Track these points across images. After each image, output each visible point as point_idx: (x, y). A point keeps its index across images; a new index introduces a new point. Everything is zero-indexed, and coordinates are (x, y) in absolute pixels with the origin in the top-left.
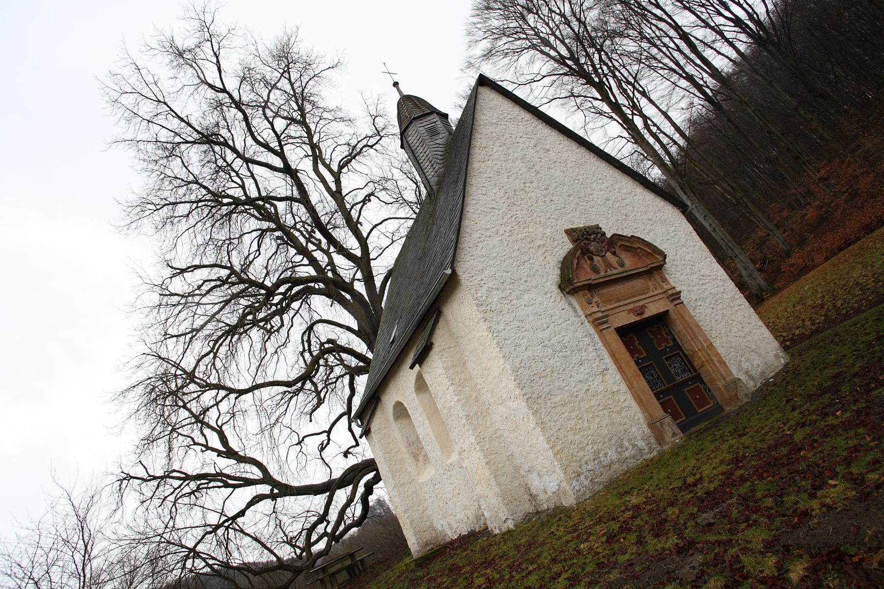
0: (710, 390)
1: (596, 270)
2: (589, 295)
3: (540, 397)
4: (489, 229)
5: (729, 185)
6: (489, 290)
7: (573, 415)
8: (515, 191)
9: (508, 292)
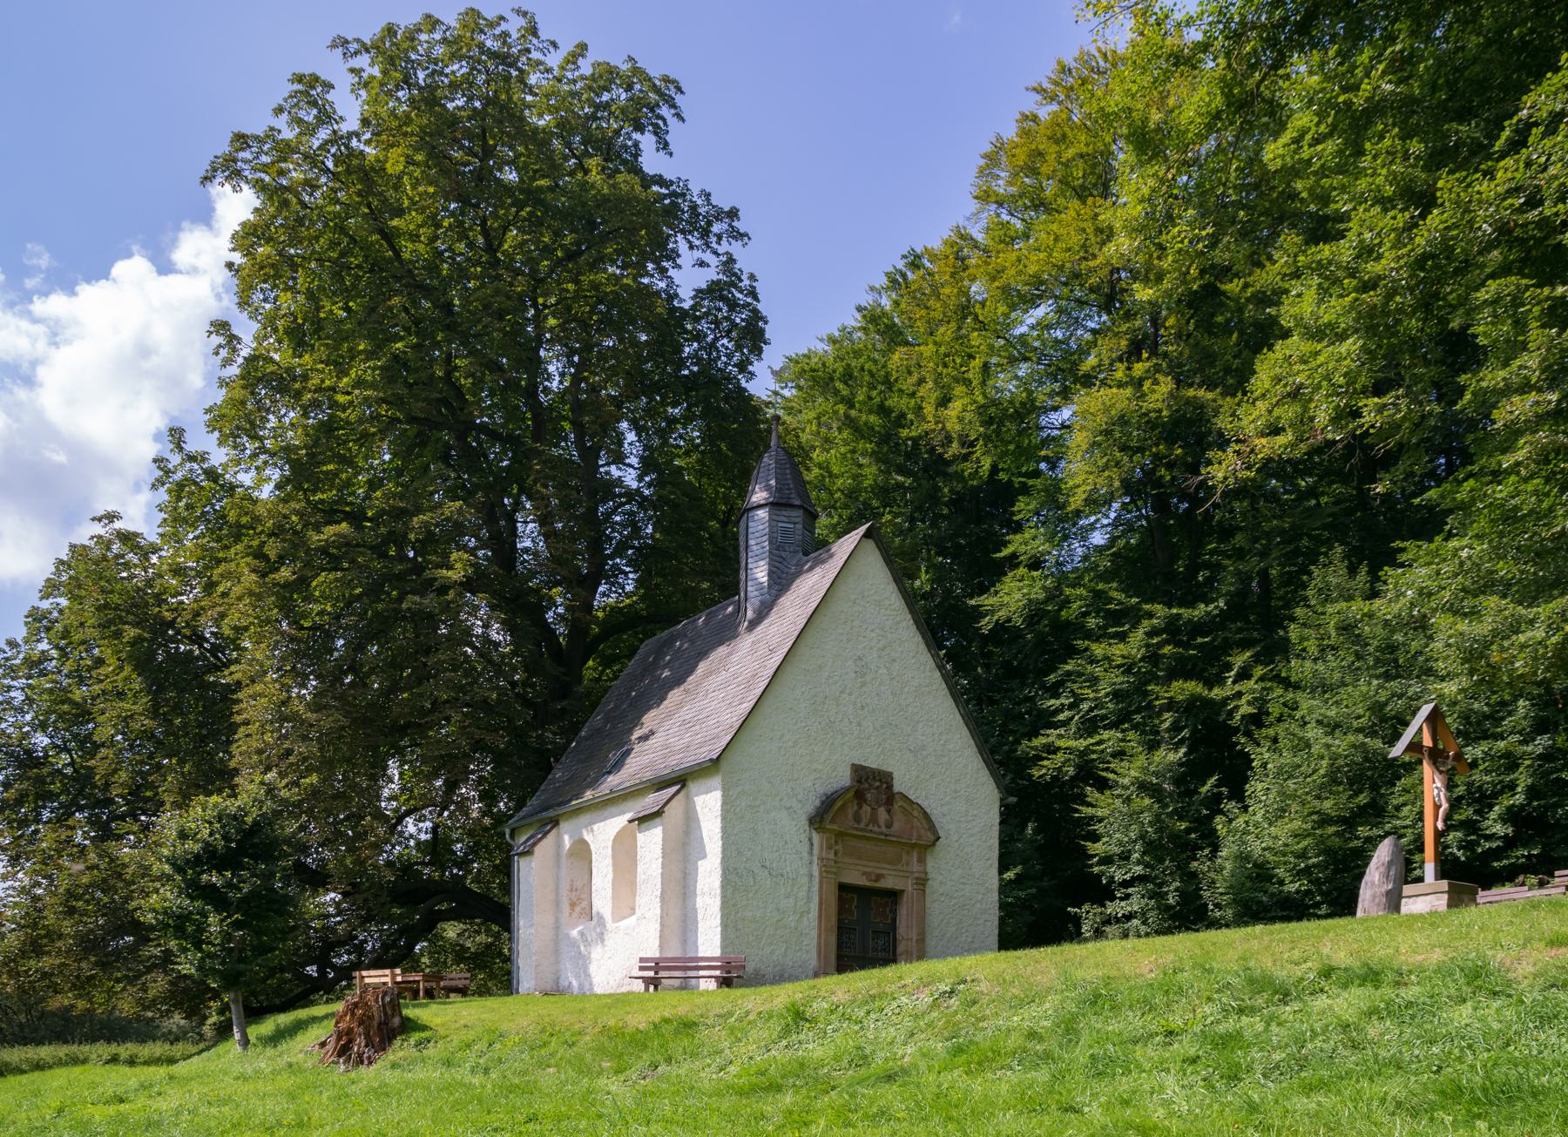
1: (857, 819)
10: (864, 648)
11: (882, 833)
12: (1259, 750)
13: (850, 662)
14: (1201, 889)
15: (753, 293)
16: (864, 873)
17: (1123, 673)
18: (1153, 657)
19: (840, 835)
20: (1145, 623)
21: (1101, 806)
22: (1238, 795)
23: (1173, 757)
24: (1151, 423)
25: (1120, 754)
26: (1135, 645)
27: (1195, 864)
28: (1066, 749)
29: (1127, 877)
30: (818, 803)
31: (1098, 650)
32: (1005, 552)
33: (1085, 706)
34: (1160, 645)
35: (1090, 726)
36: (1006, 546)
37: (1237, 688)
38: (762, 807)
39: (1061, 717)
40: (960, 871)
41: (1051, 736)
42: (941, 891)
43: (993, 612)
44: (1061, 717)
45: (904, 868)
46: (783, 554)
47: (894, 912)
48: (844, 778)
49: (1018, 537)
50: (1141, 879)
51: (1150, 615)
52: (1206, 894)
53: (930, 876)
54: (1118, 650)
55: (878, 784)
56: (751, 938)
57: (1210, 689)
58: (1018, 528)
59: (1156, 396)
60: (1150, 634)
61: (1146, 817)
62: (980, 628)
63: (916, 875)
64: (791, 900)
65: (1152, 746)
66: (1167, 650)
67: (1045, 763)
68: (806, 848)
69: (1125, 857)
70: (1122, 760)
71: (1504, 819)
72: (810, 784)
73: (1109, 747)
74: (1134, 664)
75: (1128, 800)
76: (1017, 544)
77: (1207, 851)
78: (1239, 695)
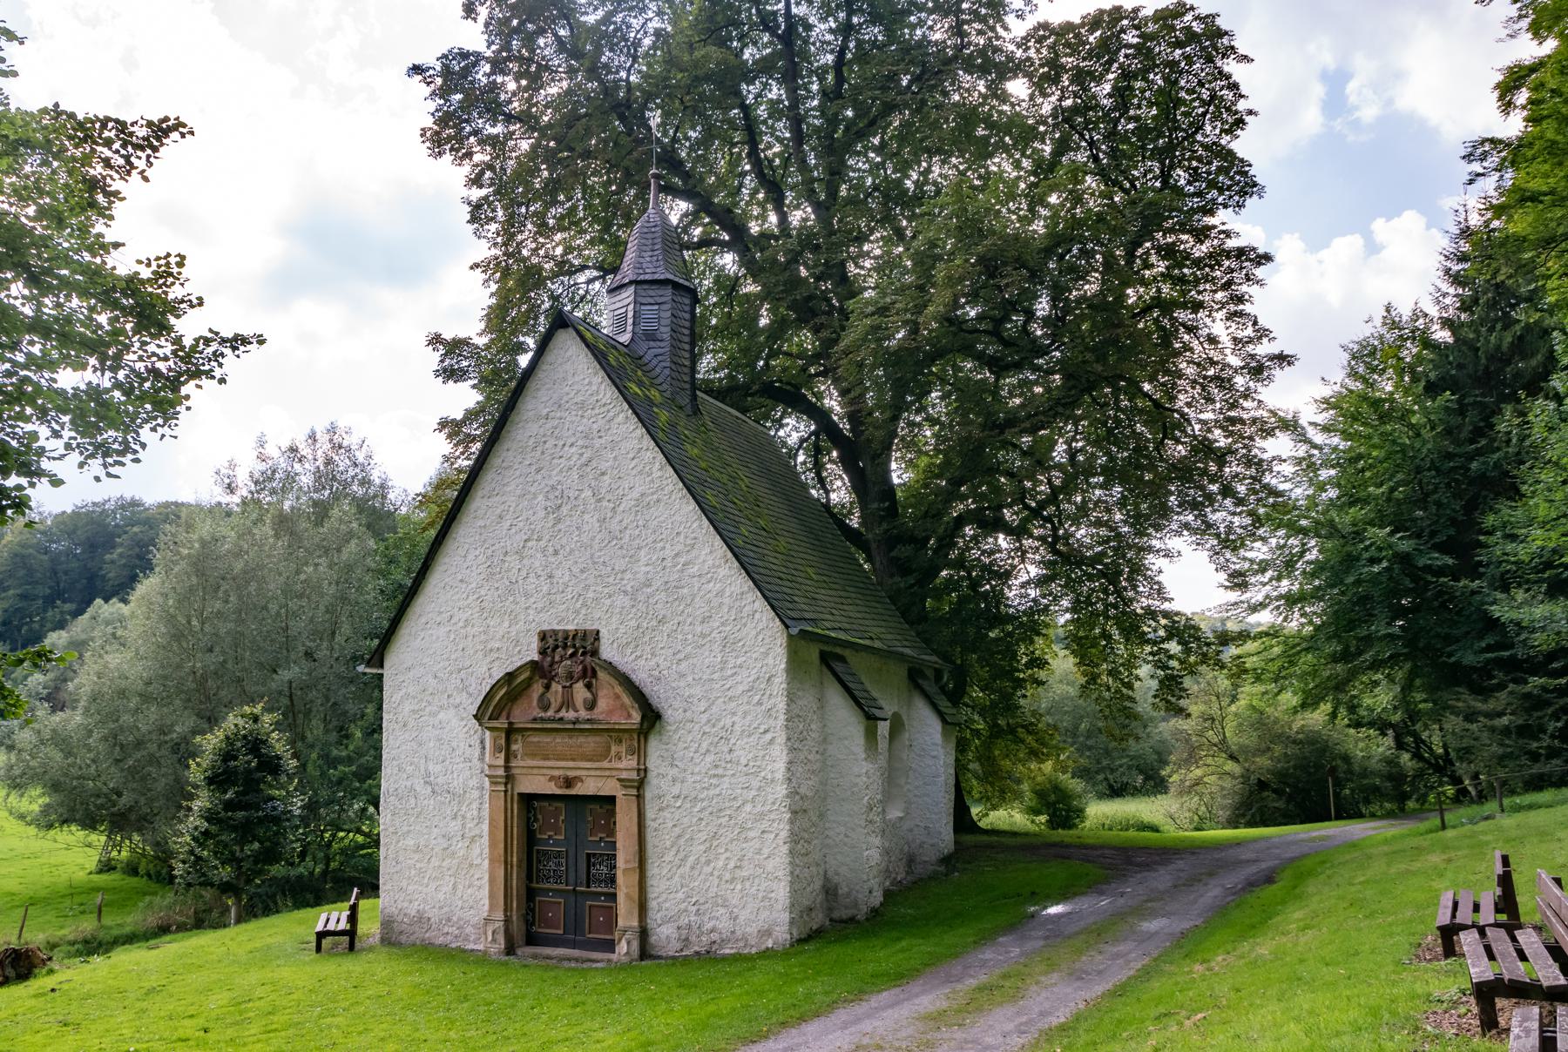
16: (552, 778)
42: (675, 791)
48: (530, 652)
56: (413, 872)
68: (477, 753)
72: (485, 668)
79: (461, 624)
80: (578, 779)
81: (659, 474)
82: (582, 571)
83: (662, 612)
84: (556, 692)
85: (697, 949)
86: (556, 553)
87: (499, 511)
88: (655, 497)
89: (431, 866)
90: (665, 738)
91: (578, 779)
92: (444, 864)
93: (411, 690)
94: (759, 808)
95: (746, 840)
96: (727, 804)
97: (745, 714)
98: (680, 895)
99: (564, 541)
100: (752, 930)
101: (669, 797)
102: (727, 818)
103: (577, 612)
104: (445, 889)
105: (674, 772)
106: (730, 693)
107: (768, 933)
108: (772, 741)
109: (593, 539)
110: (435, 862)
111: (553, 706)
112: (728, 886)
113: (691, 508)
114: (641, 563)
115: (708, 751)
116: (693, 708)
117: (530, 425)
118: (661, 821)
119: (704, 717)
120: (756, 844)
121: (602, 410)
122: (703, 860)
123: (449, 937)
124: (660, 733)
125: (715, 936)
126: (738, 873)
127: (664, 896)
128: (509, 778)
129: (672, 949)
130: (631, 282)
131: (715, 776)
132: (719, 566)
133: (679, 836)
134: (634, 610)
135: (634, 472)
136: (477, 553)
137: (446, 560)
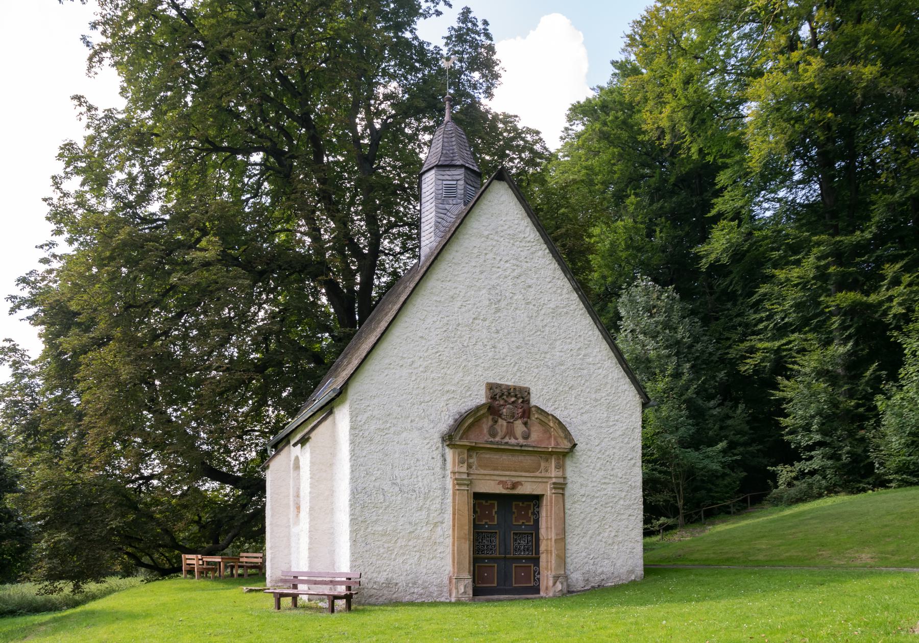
0: (539, 573)
1: (493, 434)
2: (466, 456)
3: (366, 521)
4: (405, 358)
5: (246, 557)
6: (372, 417)
7: (386, 545)
8: (459, 325)
9: (388, 425)
10: (499, 277)
11: (518, 445)
12: (909, 340)
13: (484, 291)
14: (869, 451)
15: (488, 36)
16: (501, 482)
17: (801, 289)
18: (822, 275)
19: (471, 449)
20: (815, 250)
21: (788, 389)
22: (893, 377)
23: (842, 350)
24: (807, 94)
25: (802, 351)
26: (809, 266)
27: (862, 432)
28: (764, 349)
29: (810, 443)
30: (451, 421)
31: (781, 274)
32: (713, 212)
33: (778, 317)
34: (827, 266)
35: (782, 330)
36: (713, 208)
37: (890, 293)
38: (392, 430)
39: (761, 326)
40: (601, 473)
41: (754, 341)
42: (582, 492)
43: (707, 256)
44: (761, 326)
45: (543, 474)
46: (447, 207)
47: (537, 514)
48: (480, 398)
49: (720, 199)
50: (820, 444)
51: (818, 244)
52: (873, 455)
53: (569, 481)
54: (795, 273)
55: (513, 399)
56: (382, 550)
57: (868, 296)
58: (719, 193)
59: (809, 74)
60: (819, 259)
61: (823, 397)
62: (700, 268)
63: (554, 480)
64: (424, 512)
65: (827, 343)
66: (832, 269)
67: (748, 361)
68: (439, 463)
69: (807, 428)
70: (804, 355)
71: (721, 162)
72: (443, 404)
73: (795, 346)
74: (808, 282)
75: (809, 385)
76: (720, 205)
77: (872, 422)
78: (890, 299)
79: (421, 369)
80: (519, 483)
81: (567, 296)
82: (518, 348)
83: (572, 383)
84: (502, 425)
85: (593, 584)
86: (498, 332)
87: (451, 293)
88: (565, 310)
89: (398, 545)
90: (575, 460)
91: (519, 483)
92: (410, 543)
93: (376, 413)
94: (627, 502)
95: (621, 520)
96: (611, 500)
97: (621, 448)
98: (584, 554)
99: (503, 325)
100: (624, 570)
101: (578, 495)
102: (610, 508)
103: (515, 375)
104: (410, 562)
105: (581, 480)
106: (611, 436)
107: (631, 572)
108: (634, 465)
109: (524, 328)
110: (402, 542)
111: (499, 434)
112: (610, 547)
113: (588, 322)
114: (556, 350)
115: (601, 468)
116: (592, 443)
117: (473, 238)
118: (573, 510)
119: (598, 448)
120: (625, 523)
121: (528, 244)
122: (597, 532)
123: (415, 596)
124: (572, 457)
125: (603, 577)
126: (617, 539)
127: (575, 555)
128: (470, 483)
129: (580, 585)
130: (462, 166)
131: (605, 483)
132: (605, 361)
133: (584, 519)
134: (554, 379)
135: (551, 291)
136: (435, 319)
137: (406, 319)
